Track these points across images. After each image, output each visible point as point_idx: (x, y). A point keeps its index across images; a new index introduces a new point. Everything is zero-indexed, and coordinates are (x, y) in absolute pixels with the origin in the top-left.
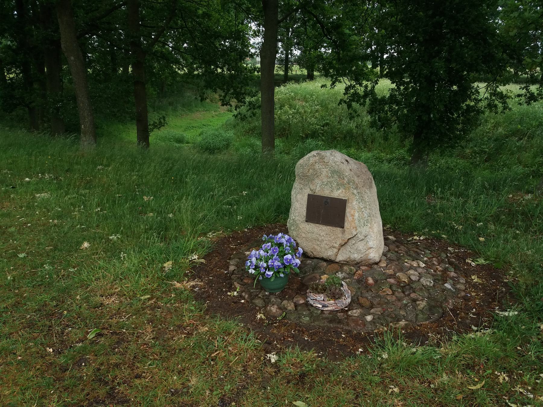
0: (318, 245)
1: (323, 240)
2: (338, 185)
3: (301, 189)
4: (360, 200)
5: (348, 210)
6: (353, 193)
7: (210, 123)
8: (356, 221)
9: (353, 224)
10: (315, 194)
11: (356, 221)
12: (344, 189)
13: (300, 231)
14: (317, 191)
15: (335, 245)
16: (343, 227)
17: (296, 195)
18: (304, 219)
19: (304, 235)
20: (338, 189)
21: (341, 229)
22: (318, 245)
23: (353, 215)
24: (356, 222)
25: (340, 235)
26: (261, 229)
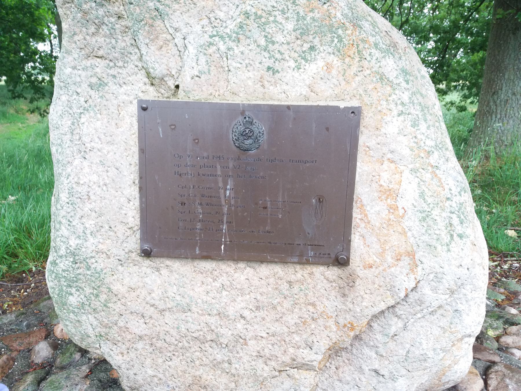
0: (216, 365)
1: (241, 340)
2: (302, 33)
3: (99, 85)
4: (416, 111)
5: (363, 168)
6: (382, 78)
7: (16, 136)
8: (411, 222)
9: (395, 240)
10: (181, 97)
11: (411, 222)
12: (340, 53)
13: (118, 307)
14: (185, 81)
15: (306, 355)
16: (342, 262)
17: (76, 123)
18: (134, 242)
19: (137, 327)
20: (306, 56)
21: (333, 272)
22: (216, 365)
23: (389, 194)
24: (407, 223)
25: (331, 303)
26: (21, 280)
